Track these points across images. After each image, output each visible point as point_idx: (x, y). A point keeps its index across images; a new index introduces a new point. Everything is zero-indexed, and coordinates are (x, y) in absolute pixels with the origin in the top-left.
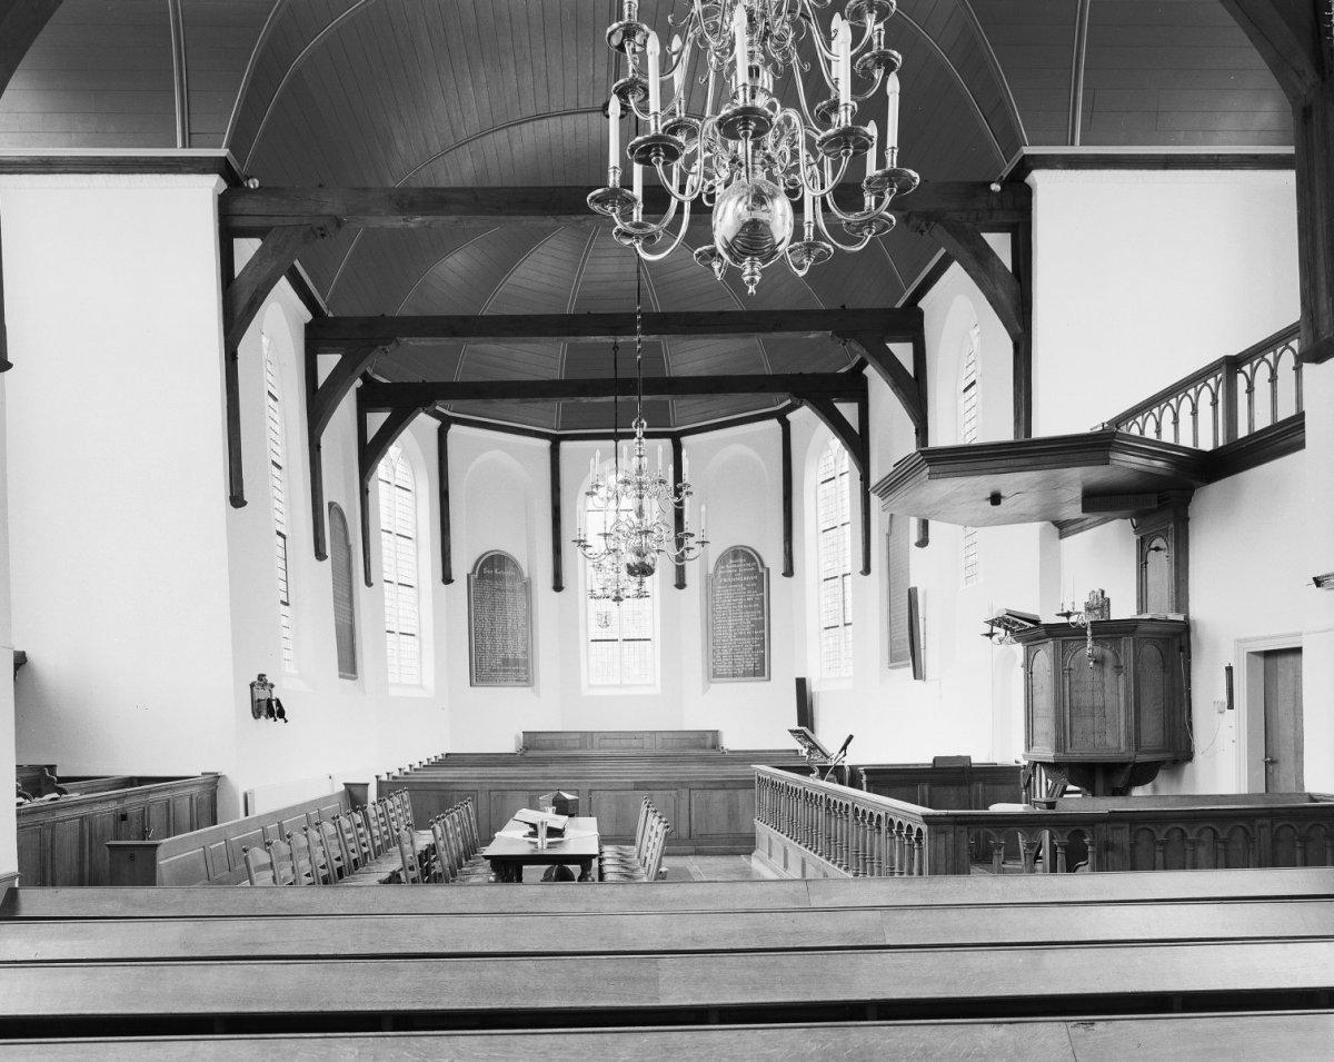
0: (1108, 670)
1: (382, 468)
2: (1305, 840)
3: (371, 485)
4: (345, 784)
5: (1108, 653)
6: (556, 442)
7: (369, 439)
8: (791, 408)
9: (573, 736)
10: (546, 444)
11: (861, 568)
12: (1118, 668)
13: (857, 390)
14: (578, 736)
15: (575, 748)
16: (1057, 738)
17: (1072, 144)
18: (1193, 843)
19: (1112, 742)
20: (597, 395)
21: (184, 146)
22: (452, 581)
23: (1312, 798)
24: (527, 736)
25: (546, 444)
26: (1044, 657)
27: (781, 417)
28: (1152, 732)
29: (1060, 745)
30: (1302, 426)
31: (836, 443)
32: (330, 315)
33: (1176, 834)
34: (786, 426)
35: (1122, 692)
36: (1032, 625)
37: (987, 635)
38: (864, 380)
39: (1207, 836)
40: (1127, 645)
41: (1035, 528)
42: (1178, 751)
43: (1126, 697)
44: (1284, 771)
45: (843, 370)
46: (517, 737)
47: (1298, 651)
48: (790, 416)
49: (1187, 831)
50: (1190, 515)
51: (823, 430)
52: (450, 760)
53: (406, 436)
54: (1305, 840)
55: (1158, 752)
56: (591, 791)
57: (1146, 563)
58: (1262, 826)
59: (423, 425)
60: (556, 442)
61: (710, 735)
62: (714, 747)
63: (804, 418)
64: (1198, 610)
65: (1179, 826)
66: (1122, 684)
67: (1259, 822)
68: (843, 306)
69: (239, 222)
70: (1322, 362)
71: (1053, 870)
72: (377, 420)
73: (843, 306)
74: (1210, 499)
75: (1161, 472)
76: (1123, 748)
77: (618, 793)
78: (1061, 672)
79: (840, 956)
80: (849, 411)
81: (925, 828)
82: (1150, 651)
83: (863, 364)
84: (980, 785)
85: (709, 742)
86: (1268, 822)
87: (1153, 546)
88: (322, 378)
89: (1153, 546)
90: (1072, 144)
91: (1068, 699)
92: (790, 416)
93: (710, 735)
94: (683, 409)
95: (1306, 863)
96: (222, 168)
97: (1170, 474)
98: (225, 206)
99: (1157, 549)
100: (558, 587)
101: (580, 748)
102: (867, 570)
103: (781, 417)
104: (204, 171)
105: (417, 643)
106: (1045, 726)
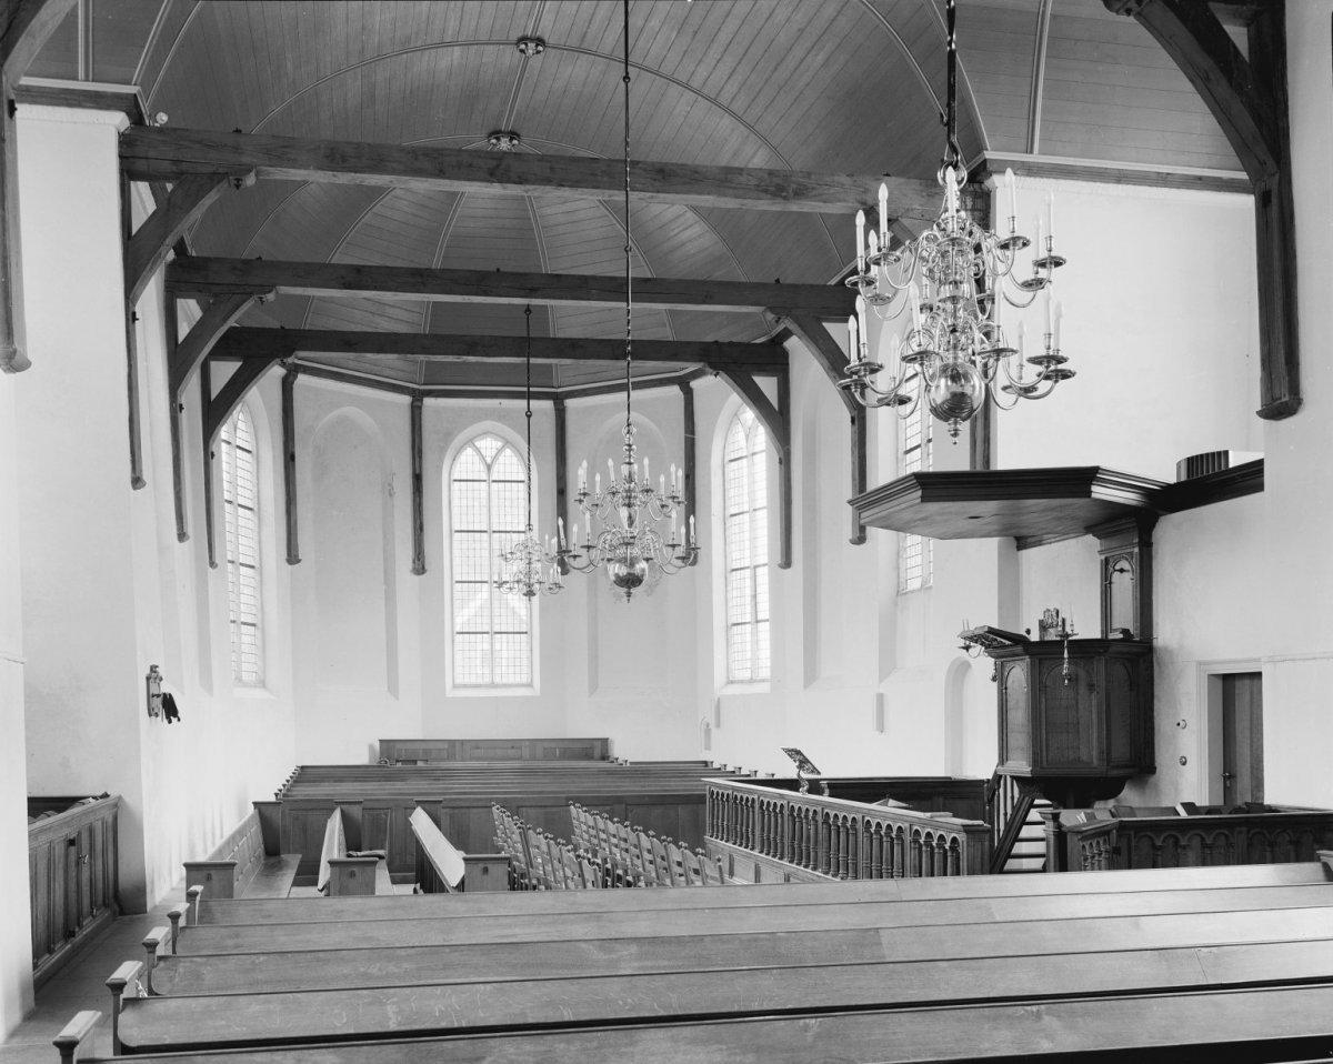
0: (1083, 690)
1: (224, 432)
2: (1272, 845)
3: (214, 448)
4: (255, 804)
5: (1082, 673)
6: (417, 397)
7: (213, 396)
8: (696, 375)
9: (440, 746)
10: (406, 400)
11: (778, 559)
12: (1091, 687)
13: (774, 359)
14: (527, 743)
15: (443, 760)
16: (1034, 753)
17: (1031, 152)
18: (1184, 847)
19: (1088, 751)
20: (488, 355)
21: (87, 80)
22: (299, 561)
23: (1270, 809)
24: (385, 744)
25: (406, 400)
26: (1019, 674)
27: (684, 383)
28: (1121, 750)
29: (1036, 761)
30: (1261, 471)
31: (749, 415)
32: (194, 254)
33: (1171, 841)
34: (689, 394)
35: (1094, 710)
36: (1007, 642)
37: (963, 648)
38: (785, 355)
39: (1196, 842)
40: (1100, 666)
41: (993, 543)
42: (1141, 764)
43: (1099, 713)
44: (1244, 782)
45: (758, 341)
46: (371, 747)
47: (1259, 675)
48: (694, 384)
49: (1180, 837)
50: (1154, 540)
51: (735, 398)
52: (304, 775)
53: (253, 394)
54: (1272, 845)
55: (1126, 767)
56: (518, 807)
57: (1110, 583)
58: (1240, 832)
59: (276, 372)
60: (417, 397)
61: (599, 744)
62: (605, 757)
63: (713, 388)
64: (1165, 634)
65: (1174, 833)
66: (1094, 702)
67: (1238, 829)
68: (778, 281)
69: (141, 165)
70: (1280, 419)
71: (1100, 869)
72: (224, 371)
73: (778, 281)
74: (1172, 530)
75: (1134, 503)
76: (1095, 762)
77: (548, 810)
78: (1038, 687)
79: (550, 1037)
80: (767, 385)
81: (962, 837)
82: (1120, 671)
83: (787, 334)
84: (941, 799)
85: (597, 753)
86: (1244, 829)
87: (1117, 567)
88: (183, 331)
89: (1117, 567)
90: (1031, 152)
91: (1044, 715)
92: (694, 384)
93: (599, 744)
94: (566, 369)
95: (1273, 861)
96: (132, 107)
97: (1140, 504)
98: (125, 141)
99: (1122, 571)
100: (420, 567)
101: (449, 759)
102: (787, 562)
103: (684, 383)
104: (108, 107)
105: (258, 634)
106: (1020, 740)
